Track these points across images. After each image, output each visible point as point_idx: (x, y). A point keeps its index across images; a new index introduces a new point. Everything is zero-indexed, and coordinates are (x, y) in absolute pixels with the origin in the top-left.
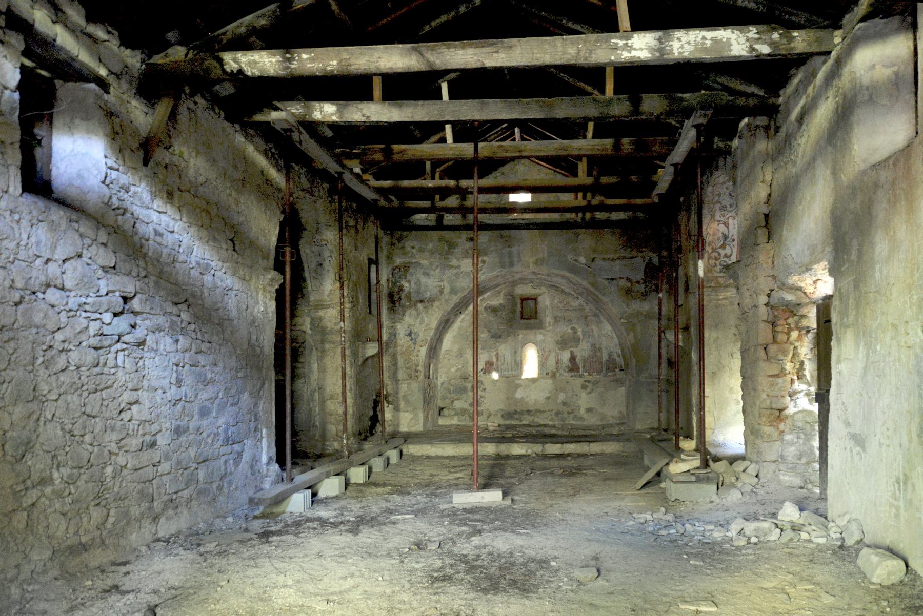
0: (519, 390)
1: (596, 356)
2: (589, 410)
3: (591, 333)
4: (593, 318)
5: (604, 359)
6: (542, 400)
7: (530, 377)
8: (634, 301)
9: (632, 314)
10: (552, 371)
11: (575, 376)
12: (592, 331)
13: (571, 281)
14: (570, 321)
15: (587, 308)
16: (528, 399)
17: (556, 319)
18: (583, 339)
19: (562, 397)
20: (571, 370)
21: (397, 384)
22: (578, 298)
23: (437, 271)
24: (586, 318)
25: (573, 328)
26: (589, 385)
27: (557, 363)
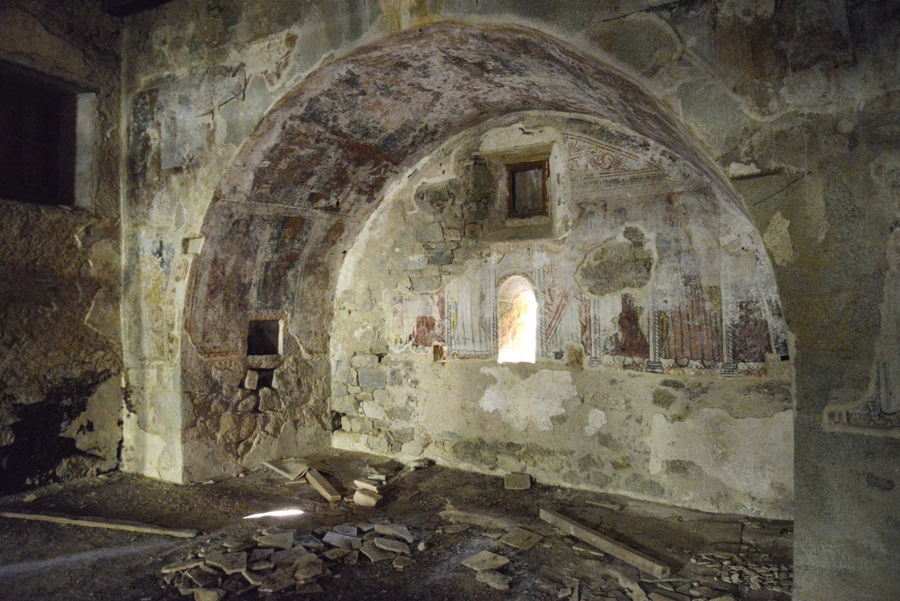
0: (488, 392)
1: (701, 311)
2: (676, 467)
3: (684, 245)
4: (691, 200)
5: (727, 322)
6: (543, 423)
7: (516, 359)
8: (790, 78)
9: (781, 136)
10: (571, 349)
11: (635, 366)
12: (689, 237)
13: (660, 123)
14: (621, 212)
15: (674, 174)
16: (511, 415)
17: (583, 211)
18: (661, 261)
19: (596, 419)
20: (622, 349)
21: (143, 367)
22: (645, 146)
23: (203, 88)
24: (669, 200)
25: (629, 233)
26: (678, 394)
27: (584, 328)
